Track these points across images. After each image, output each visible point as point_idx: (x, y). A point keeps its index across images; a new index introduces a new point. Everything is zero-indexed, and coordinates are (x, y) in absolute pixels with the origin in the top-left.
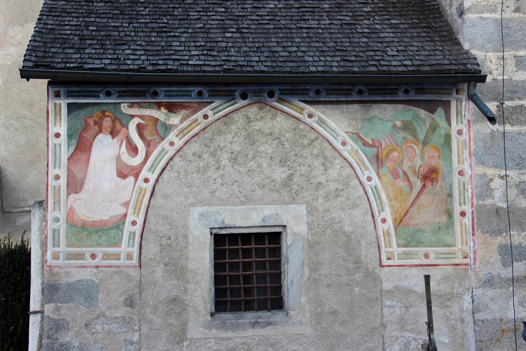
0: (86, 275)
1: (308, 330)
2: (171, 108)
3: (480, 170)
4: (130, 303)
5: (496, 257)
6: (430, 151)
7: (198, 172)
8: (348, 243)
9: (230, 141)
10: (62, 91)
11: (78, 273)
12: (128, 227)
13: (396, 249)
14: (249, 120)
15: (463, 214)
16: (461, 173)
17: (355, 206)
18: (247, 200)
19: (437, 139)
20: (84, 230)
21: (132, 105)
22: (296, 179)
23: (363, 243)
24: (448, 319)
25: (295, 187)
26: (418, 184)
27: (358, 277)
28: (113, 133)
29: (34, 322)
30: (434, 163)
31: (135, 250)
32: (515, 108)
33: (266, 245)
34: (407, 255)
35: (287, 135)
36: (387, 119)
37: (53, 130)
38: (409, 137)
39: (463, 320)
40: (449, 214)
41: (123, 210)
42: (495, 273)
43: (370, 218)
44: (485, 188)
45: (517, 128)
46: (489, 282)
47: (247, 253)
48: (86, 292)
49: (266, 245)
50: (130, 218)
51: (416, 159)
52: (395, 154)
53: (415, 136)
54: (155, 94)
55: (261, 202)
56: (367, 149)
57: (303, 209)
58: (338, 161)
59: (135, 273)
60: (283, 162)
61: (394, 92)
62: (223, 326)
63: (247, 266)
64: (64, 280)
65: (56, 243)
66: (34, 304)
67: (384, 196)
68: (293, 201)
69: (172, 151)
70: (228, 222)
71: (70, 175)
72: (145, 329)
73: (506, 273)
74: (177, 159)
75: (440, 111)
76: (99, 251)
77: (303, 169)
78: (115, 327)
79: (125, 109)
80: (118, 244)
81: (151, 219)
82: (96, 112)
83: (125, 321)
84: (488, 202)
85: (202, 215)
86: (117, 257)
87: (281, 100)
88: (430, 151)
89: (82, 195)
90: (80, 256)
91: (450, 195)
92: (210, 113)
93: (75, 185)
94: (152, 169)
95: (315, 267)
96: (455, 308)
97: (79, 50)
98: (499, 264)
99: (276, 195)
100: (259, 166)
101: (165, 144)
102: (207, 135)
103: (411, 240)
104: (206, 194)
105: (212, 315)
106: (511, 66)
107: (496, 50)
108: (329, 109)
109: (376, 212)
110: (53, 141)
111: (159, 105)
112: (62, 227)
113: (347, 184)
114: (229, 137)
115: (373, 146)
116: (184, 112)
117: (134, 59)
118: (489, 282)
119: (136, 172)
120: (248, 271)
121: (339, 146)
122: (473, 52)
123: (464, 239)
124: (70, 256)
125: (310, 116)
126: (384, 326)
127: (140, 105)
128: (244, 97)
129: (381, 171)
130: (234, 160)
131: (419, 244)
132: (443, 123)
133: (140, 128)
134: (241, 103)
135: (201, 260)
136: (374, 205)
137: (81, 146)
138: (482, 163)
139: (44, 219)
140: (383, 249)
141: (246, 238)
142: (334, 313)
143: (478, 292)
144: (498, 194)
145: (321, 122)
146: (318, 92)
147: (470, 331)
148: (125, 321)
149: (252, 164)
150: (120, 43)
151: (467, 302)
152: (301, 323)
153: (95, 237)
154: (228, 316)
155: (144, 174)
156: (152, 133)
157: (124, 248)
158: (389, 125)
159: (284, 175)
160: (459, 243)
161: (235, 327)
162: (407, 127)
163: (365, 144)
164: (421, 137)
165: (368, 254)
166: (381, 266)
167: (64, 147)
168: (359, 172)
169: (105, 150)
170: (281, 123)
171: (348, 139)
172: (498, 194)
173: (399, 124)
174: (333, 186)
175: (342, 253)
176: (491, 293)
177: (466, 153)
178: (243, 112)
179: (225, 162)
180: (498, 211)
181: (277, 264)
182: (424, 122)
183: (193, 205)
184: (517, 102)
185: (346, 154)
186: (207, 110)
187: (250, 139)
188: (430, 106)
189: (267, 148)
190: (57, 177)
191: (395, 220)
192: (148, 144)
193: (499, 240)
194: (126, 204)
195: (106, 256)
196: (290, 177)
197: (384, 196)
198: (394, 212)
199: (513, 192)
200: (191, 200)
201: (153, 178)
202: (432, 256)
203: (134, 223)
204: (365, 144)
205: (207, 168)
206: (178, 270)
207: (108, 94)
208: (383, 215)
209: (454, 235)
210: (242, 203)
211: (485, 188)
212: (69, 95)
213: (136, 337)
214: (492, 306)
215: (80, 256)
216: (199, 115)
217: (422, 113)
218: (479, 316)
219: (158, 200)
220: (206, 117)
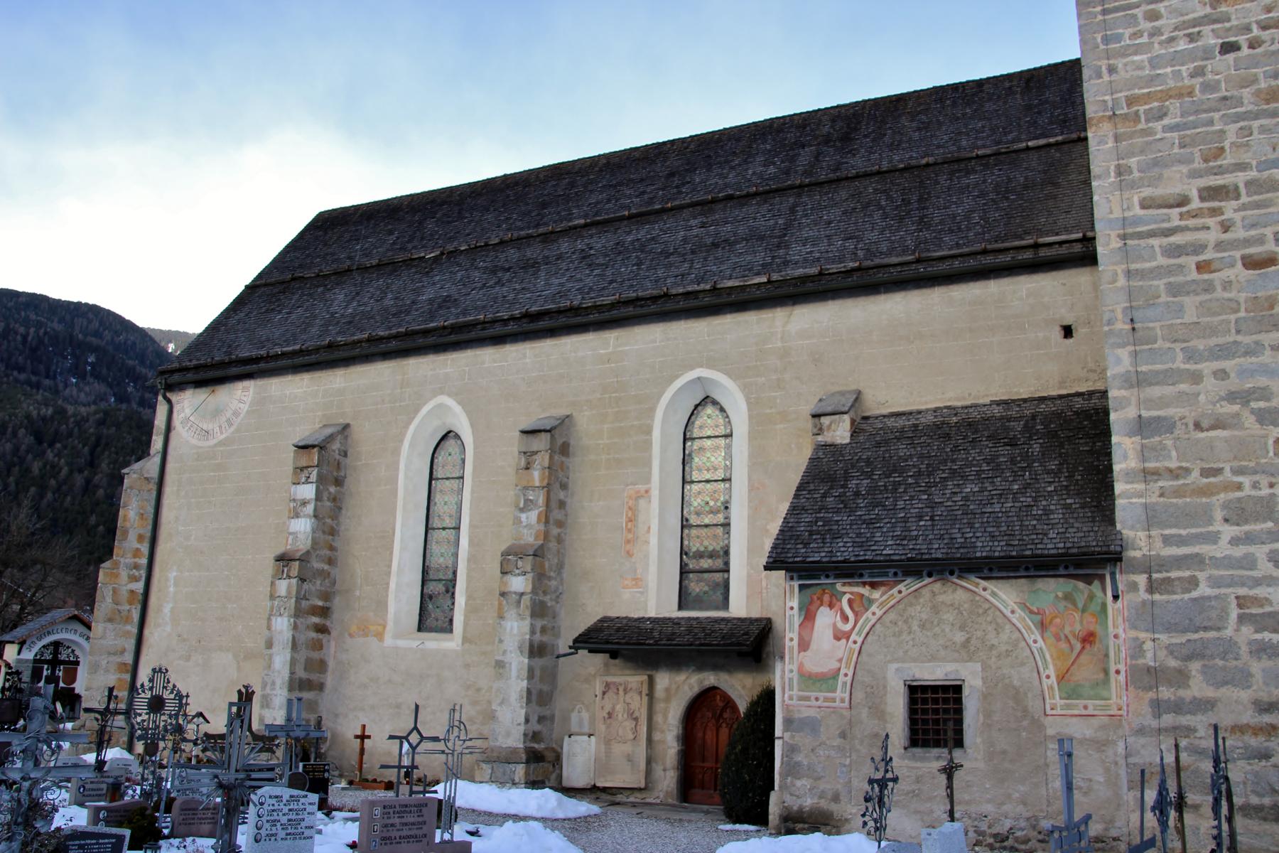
0: (811, 713)
1: (981, 765)
2: (873, 586)
3: (1133, 634)
4: (843, 735)
5: (1146, 710)
6: (1088, 618)
7: (894, 635)
8: (1017, 696)
9: (920, 611)
10: (795, 575)
11: (806, 711)
12: (841, 678)
13: (1058, 701)
14: (934, 594)
15: (1118, 672)
16: (1116, 636)
17: (1023, 664)
18: (933, 658)
19: (1095, 607)
20: (811, 680)
21: (844, 584)
22: (973, 641)
23: (1030, 695)
24: (1103, 762)
25: (972, 648)
26: (1078, 646)
27: (1025, 723)
28: (831, 606)
29: (778, 744)
30: (1092, 628)
31: (847, 696)
32: (1164, 580)
33: (951, 694)
34: (1068, 707)
35: (966, 606)
36: (1051, 590)
37: (789, 604)
38: (1070, 606)
39: (1116, 763)
40: (1106, 672)
41: (836, 665)
42: (1146, 723)
43: (1036, 674)
44: (1138, 649)
45: (1165, 597)
46: (1141, 731)
47: (936, 701)
48: (811, 725)
49: (951, 694)
50: (842, 672)
51: (1076, 624)
52: (1058, 620)
53: (1075, 604)
54: (861, 576)
55: (944, 660)
56: (1033, 616)
57: (978, 666)
58: (1008, 626)
59: (846, 713)
60: (962, 628)
61: (1055, 567)
62: (914, 758)
63: (936, 711)
64: (796, 716)
65: (791, 689)
66: (778, 733)
67: (1048, 656)
68: (970, 660)
69: (874, 619)
70: (918, 676)
71: (801, 638)
72: (854, 757)
73: (1154, 724)
74: (878, 626)
75: (1096, 583)
76: (821, 695)
77: (979, 634)
78: (833, 753)
79: (839, 587)
80: (834, 691)
81: (859, 672)
82: (819, 590)
83: (840, 749)
84: (1141, 661)
85: (897, 670)
86: (834, 700)
87: (960, 577)
88: (1088, 618)
89: (808, 653)
90: (808, 699)
91: (1107, 656)
92: (903, 589)
93: (804, 645)
94: (859, 634)
95: (988, 714)
96: (1110, 752)
97: (806, 545)
98: (1149, 716)
99: (956, 655)
100: (943, 631)
101: (869, 614)
102: (901, 606)
103: (1072, 693)
104: (901, 653)
105: (905, 749)
106: (1158, 543)
107: (1144, 530)
108: (1000, 583)
109: (1041, 669)
110: (788, 612)
111: (864, 584)
112: (795, 675)
113: (1016, 646)
114: (918, 608)
115: (1038, 613)
116: (883, 589)
117: (844, 550)
118: (1141, 731)
119: (847, 636)
120: (935, 715)
121: (1009, 615)
122: (252, 810)
123: (1118, 695)
124: (801, 698)
125: (985, 589)
126: (1047, 765)
127: (850, 584)
128: (930, 575)
129: (1046, 635)
130: (923, 626)
131: (1079, 697)
132: (1099, 594)
133: (850, 602)
134: (927, 580)
135: (897, 706)
136: (1040, 663)
137: (808, 616)
138: (1134, 627)
139: (783, 671)
140: (1048, 701)
141: (935, 689)
142: (1004, 752)
143: (1131, 740)
144: (1149, 655)
145: (994, 594)
146: (991, 570)
147: (1123, 772)
148: (840, 749)
149: (937, 630)
150: (836, 536)
151: (1121, 748)
152: (976, 759)
153: (818, 685)
154: (918, 751)
155: (853, 637)
156: (861, 605)
157: (838, 694)
158: (1053, 595)
159: (963, 639)
160: (1114, 696)
161: (923, 759)
162: (1068, 597)
163: (1031, 612)
164: (1080, 605)
165: (1034, 705)
166: (1046, 715)
167: (796, 618)
168: (1026, 635)
169: (825, 618)
170: (960, 596)
171: (1016, 607)
172: (1149, 655)
173: (1060, 594)
174: (1003, 648)
175: (1011, 703)
176: (1142, 740)
177: (1120, 619)
178: (929, 587)
179: (915, 628)
180: (1149, 669)
181: (959, 711)
182: (1082, 592)
183: (889, 662)
184: (1165, 575)
185: (1014, 621)
186: (901, 587)
187: (936, 609)
188: (1088, 579)
189: (949, 616)
190: (792, 640)
191: (1057, 677)
192: (857, 614)
193: (1151, 695)
194: (840, 660)
195: (826, 700)
196: (968, 641)
197: (1048, 656)
198: (1057, 670)
199: (1162, 654)
200: (889, 658)
201: (860, 640)
202: (1091, 707)
203: (846, 675)
204: (1031, 612)
205: (901, 633)
206: (878, 712)
207: (827, 577)
208: (1047, 672)
209: (1109, 690)
210: (929, 661)
211: (1138, 649)
212: (800, 578)
213: (848, 762)
214: (1143, 752)
215: (808, 699)
216: (895, 590)
217: (1081, 585)
218: (1131, 760)
219: (864, 657)
220: (900, 592)
